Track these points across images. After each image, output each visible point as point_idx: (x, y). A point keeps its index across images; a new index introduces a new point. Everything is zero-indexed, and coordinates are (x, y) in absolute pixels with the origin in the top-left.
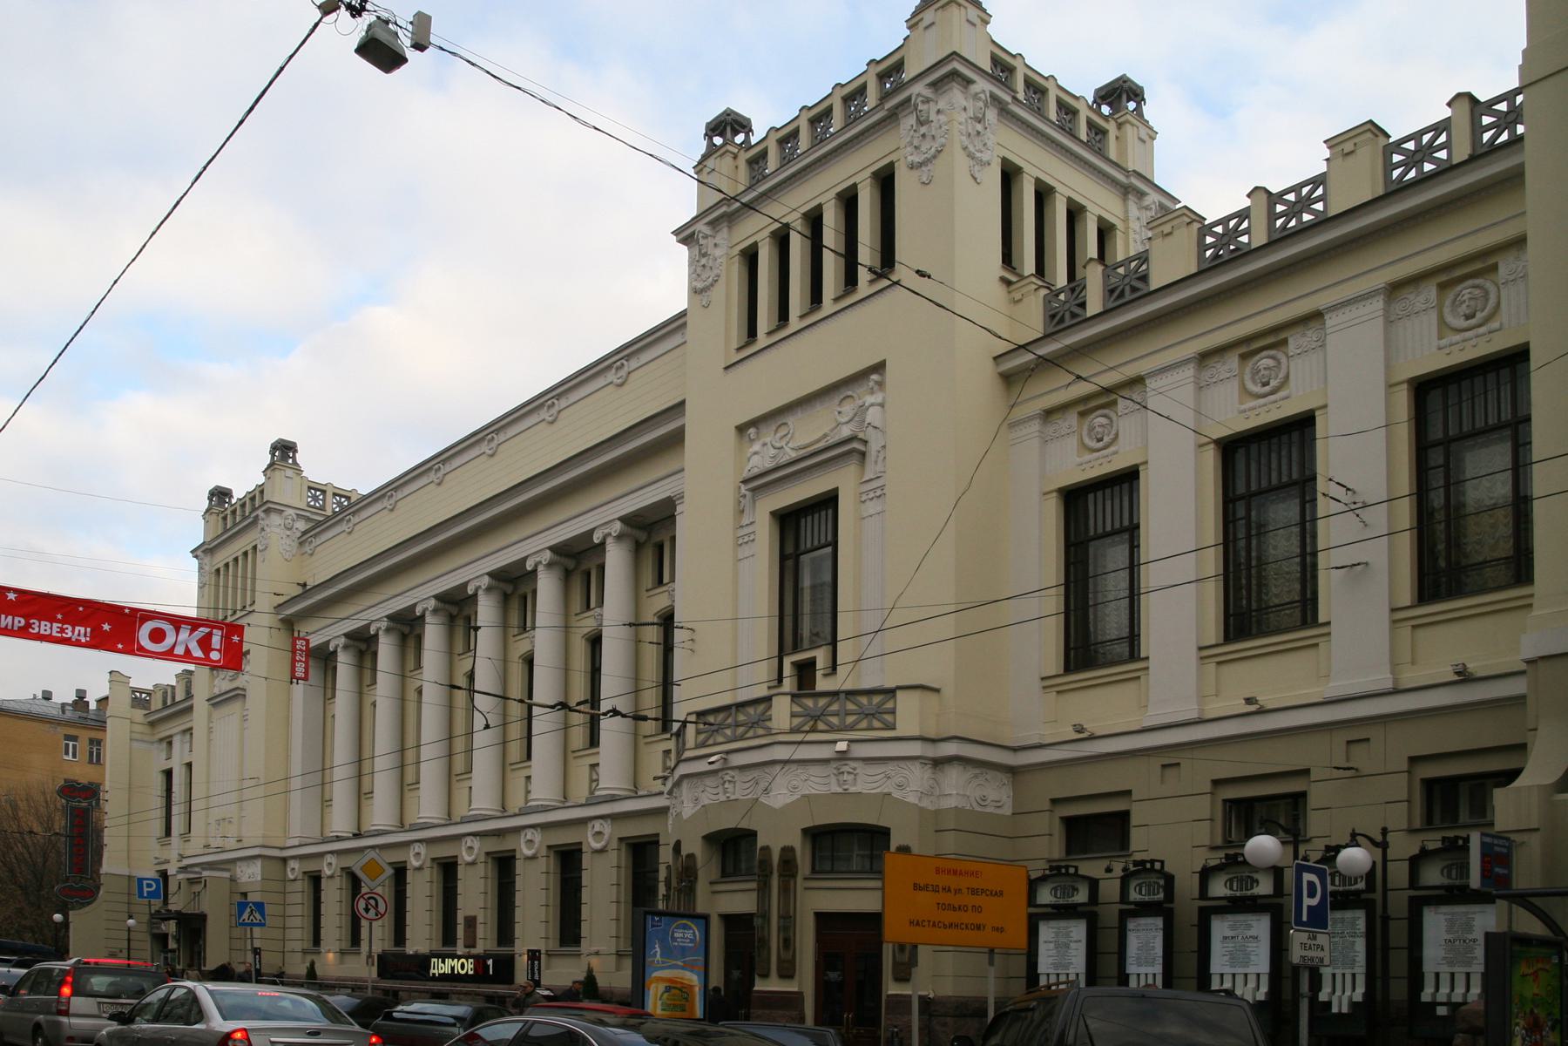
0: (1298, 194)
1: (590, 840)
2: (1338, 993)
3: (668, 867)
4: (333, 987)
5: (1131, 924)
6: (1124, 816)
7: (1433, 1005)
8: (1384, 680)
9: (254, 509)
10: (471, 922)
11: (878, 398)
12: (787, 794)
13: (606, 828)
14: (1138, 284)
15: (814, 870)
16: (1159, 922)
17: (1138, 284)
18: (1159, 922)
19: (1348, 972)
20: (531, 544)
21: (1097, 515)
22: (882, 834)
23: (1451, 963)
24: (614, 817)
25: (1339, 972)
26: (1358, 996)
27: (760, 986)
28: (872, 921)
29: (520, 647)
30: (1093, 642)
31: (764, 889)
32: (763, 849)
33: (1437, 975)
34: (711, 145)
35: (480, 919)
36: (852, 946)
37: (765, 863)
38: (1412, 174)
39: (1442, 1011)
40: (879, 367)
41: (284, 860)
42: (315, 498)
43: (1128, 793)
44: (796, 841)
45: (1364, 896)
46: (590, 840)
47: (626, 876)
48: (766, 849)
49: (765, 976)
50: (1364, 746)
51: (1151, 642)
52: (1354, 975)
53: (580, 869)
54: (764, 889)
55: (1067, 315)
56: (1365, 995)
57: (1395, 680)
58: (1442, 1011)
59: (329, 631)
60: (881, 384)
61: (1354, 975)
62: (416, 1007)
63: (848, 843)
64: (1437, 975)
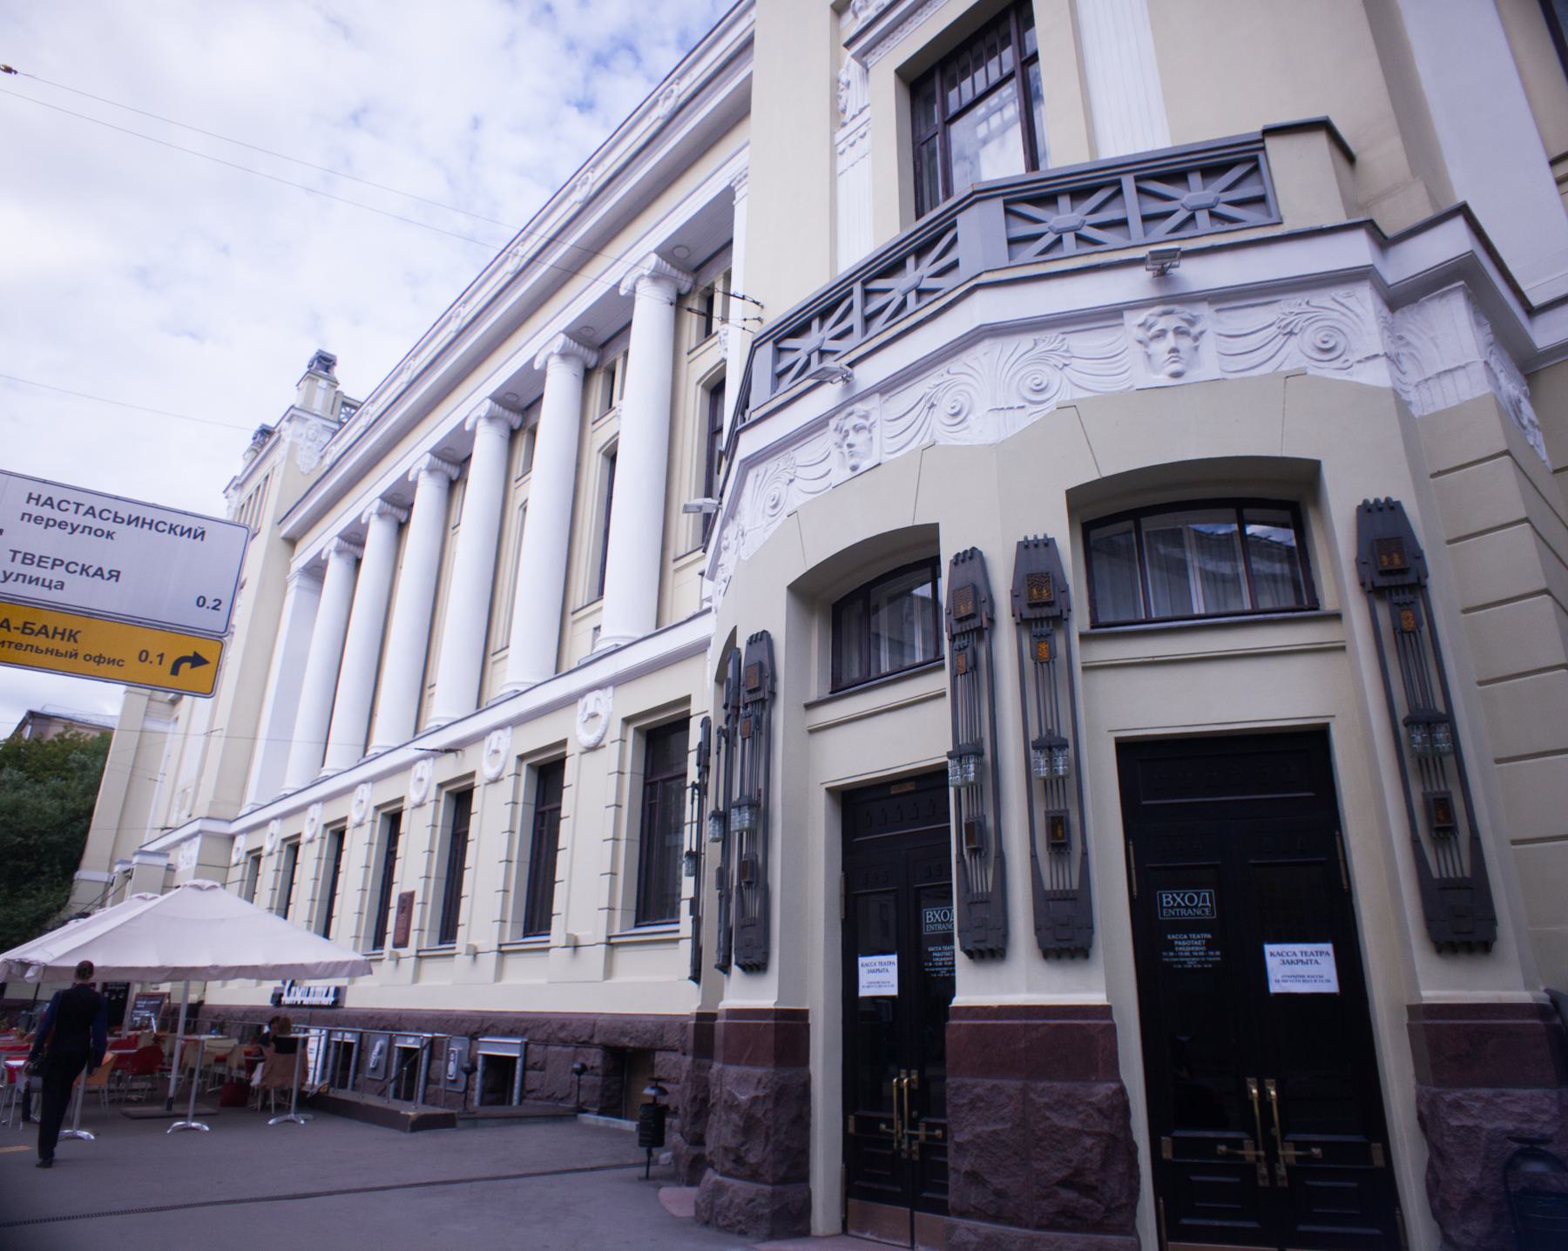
3: (706, 723)
4: (12, 1049)
10: (407, 901)
15: (1095, 624)
22: (1286, 491)
24: (618, 681)
27: (976, 988)
31: (974, 675)
32: (960, 560)
35: (418, 898)
36: (1237, 822)
37: (975, 591)
41: (232, 838)
44: (1058, 527)
47: (630, 787)
48: (970, 558)
49: (990, 949)
59: (324, 539)
62: (311, 1057)
63: (1194, 529)
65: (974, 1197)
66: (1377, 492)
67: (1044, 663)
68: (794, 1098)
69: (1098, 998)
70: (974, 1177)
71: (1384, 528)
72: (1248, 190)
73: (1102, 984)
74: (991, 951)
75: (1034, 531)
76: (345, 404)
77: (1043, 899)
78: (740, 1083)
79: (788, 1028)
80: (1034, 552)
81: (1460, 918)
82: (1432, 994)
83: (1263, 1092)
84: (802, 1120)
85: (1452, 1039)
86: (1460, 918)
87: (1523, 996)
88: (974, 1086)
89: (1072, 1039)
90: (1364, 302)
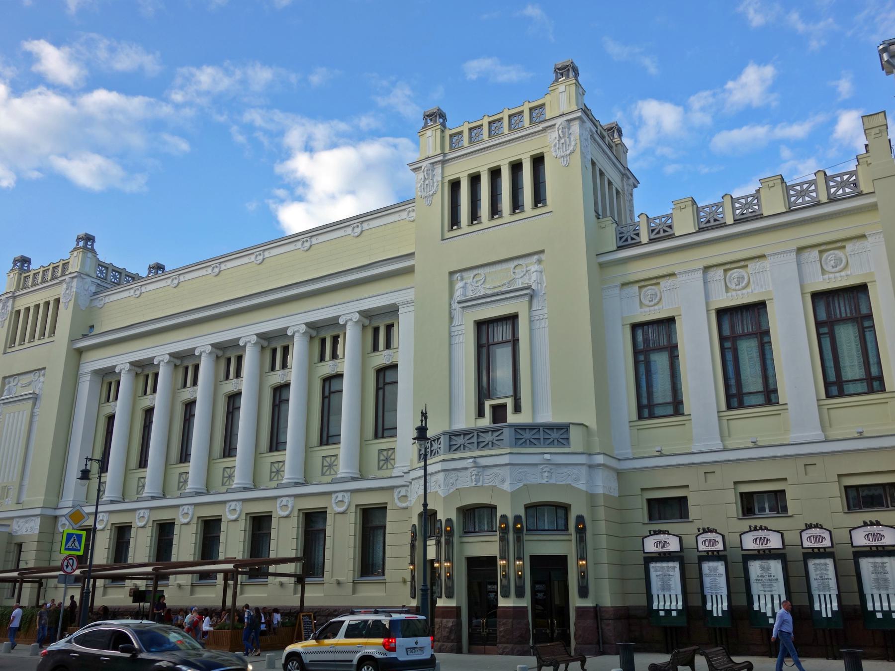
0: (802, 187)
1: (334, 505)
2: (715, 606)
5: (652, 565)
6: (684, 500)
7: (658, 610)
8: (818, 434)
9: (63, 275)
11: (42, 379)
12: (503, 479)
13: (290, 502)
14: (635, 237)
16: (677, 565)
17: (635, 237)
18: (677, 565)
19: (770, 593)
20: (202, 341)
21: (654, 339)
22: (565, 508)
23: (879, 589)
25: (822, 593)
26: (725, 608)
28: (561, 561)
29: (186, 395)
30: (657, 402)
33: (872, 595)
34: (426, 123)
36: (549, 570)
38: (840, 192)
39: (662, 613)
40: (44, 368)
42: (115, 277)
43: (785, 479)
45: (721, 553)
46: (334, 505)
50: (812, 467)
51: (689, 405)
52: (772, 596)
53: (173, 535)
54: (503, 540)
55: (662, 231)
56: (728, 606)
57: (724, 445)
58: (662, 613)
60: (44, 375)
61: (772, 596)
63: (549, 513)
64: (872, 595)
65: (503, 640)
66: (580, 514)
67: (519, 540)
68: (459, 624)
69: (525, 605)
70: (503, 636)
71: (580, 519)
72: (565, 436)
73: (525, 602)
74: (506, 595)
75: (518, 514)
76: (113, 270)
77: (517, 587)
78: (450, 622)
79: (458, 609)
80: (517, 519)
81: (583, 592)
82: (578, 605)
83: (552, 622)
84: (461, 630)
85: (581, 611)
86: (583, 592)
87: (591, 605)
88: (69, 642)
89: (518, 612)
90: (584, 470)
